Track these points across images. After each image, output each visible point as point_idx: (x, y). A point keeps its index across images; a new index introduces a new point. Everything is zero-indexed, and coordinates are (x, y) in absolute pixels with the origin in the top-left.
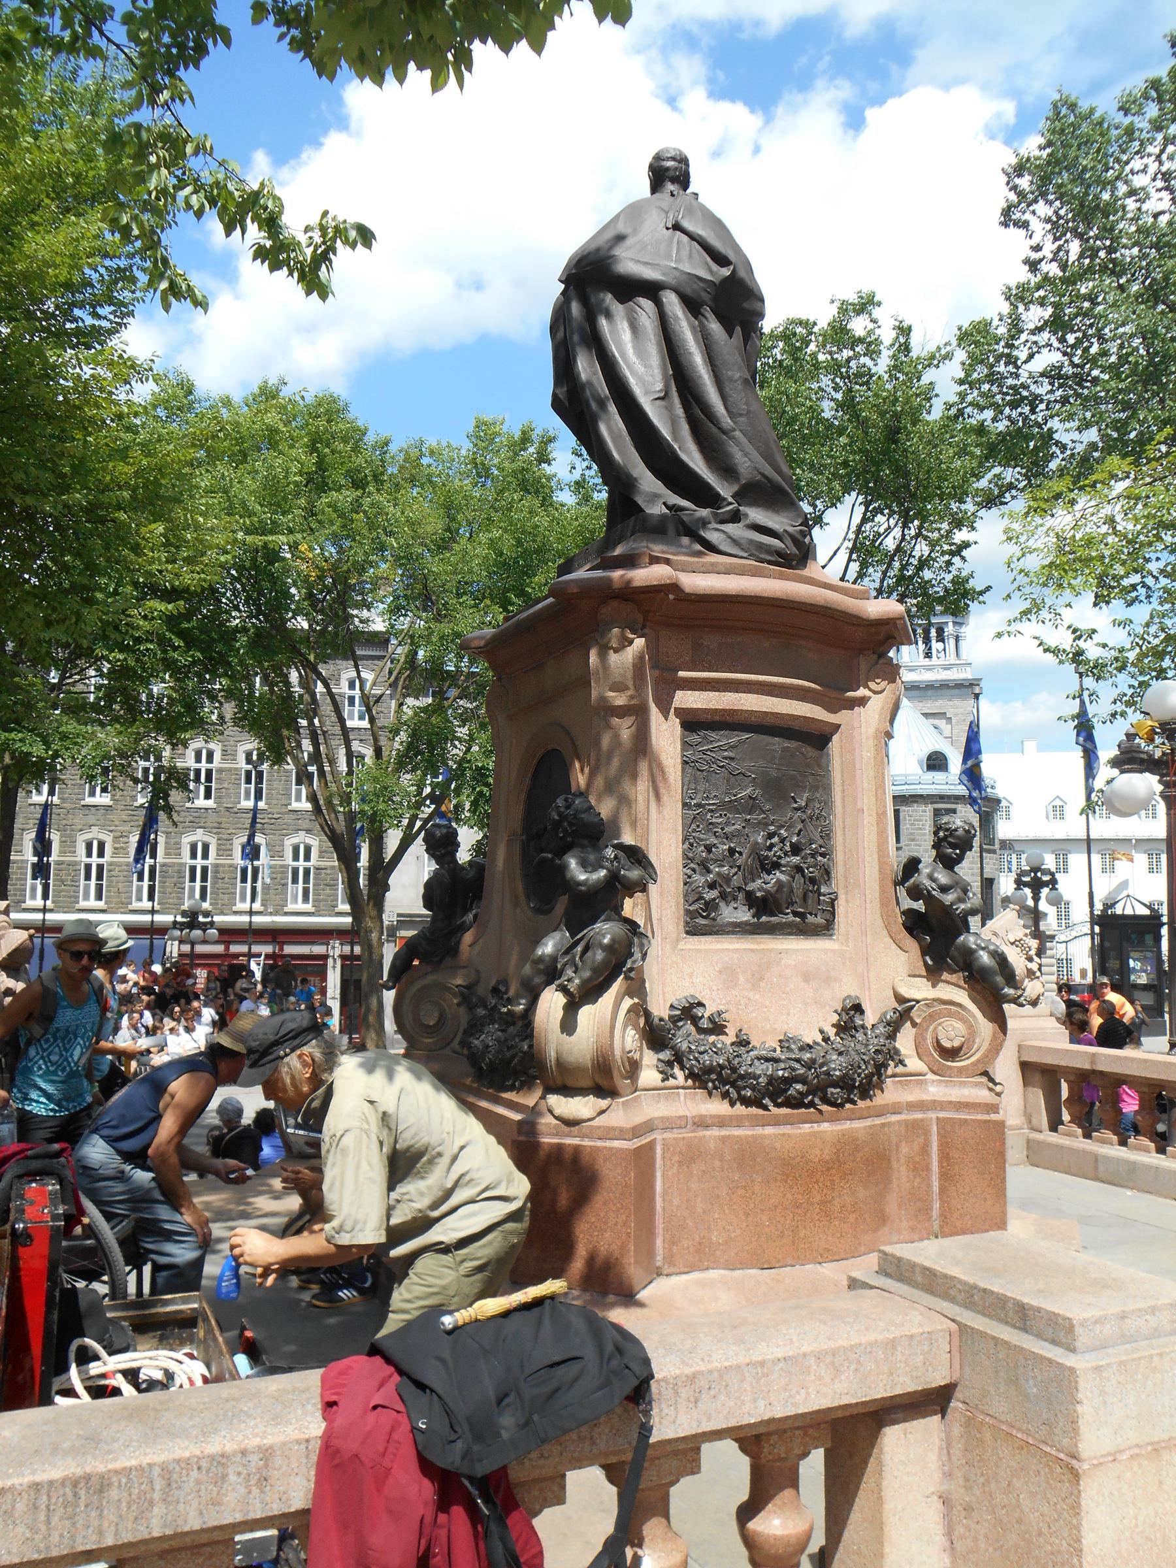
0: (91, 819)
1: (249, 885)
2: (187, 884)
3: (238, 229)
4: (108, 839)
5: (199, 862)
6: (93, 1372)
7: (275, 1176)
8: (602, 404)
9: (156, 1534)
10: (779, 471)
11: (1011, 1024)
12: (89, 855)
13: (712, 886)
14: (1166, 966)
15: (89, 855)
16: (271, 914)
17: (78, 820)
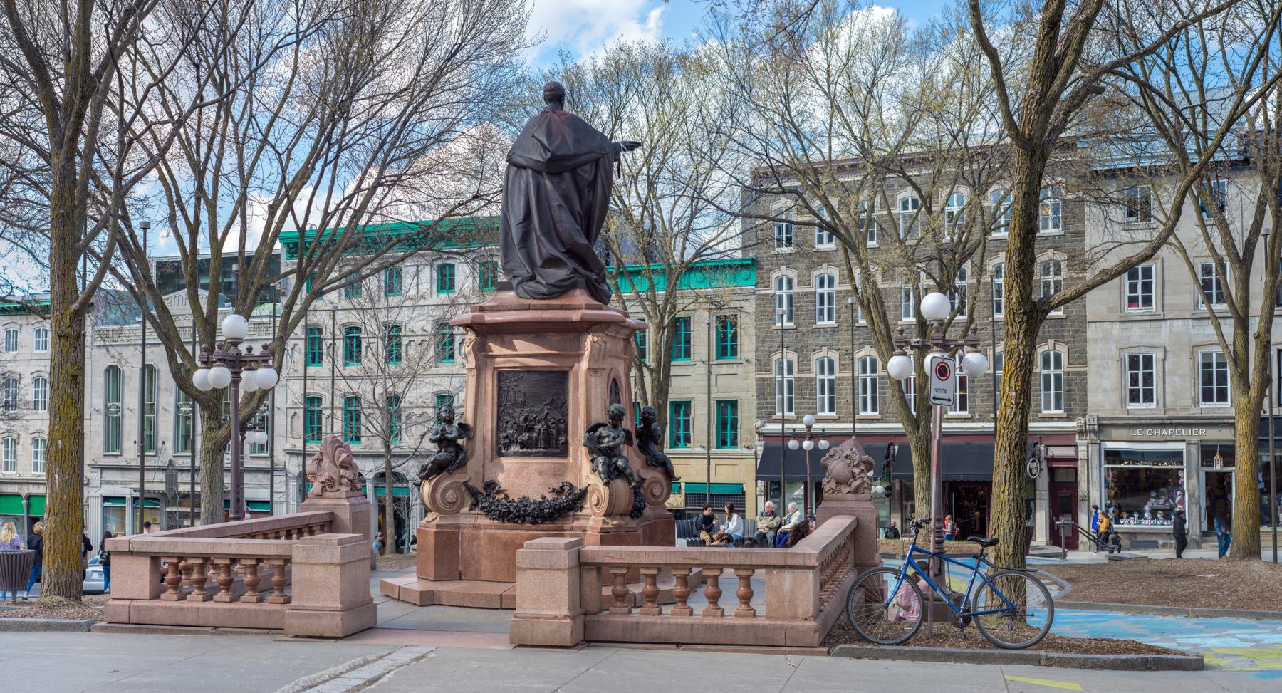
0: (822, 340)
1: (1052, 392)
2: (819, 396)
3: (1028, 582)
4: (1062, 349)
5: (826, 376)
6: (31, 398)
7: (566, 114)
8: (1266, 236)
9: (1090, 398)
10: (435, 376)
11: (678, 471)
12: (781, 372)
13: (507, 437)
14: (1273, 125)
15: (822, 371)
16: (979, 421)
17: (811, 341)
